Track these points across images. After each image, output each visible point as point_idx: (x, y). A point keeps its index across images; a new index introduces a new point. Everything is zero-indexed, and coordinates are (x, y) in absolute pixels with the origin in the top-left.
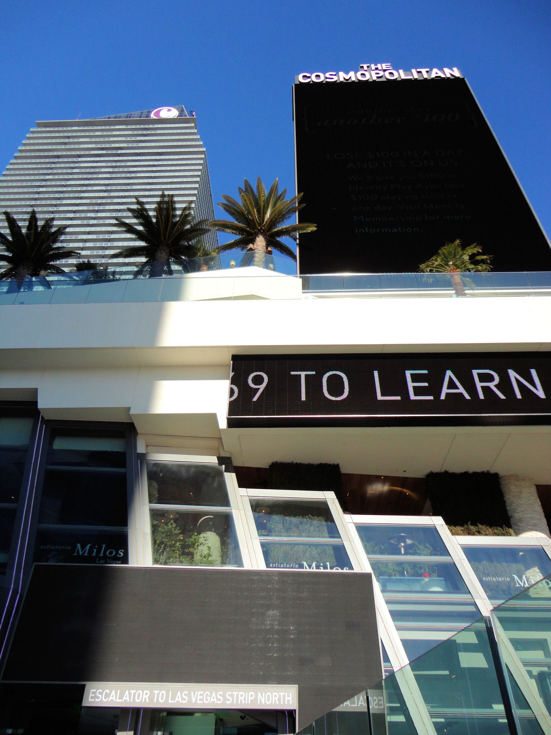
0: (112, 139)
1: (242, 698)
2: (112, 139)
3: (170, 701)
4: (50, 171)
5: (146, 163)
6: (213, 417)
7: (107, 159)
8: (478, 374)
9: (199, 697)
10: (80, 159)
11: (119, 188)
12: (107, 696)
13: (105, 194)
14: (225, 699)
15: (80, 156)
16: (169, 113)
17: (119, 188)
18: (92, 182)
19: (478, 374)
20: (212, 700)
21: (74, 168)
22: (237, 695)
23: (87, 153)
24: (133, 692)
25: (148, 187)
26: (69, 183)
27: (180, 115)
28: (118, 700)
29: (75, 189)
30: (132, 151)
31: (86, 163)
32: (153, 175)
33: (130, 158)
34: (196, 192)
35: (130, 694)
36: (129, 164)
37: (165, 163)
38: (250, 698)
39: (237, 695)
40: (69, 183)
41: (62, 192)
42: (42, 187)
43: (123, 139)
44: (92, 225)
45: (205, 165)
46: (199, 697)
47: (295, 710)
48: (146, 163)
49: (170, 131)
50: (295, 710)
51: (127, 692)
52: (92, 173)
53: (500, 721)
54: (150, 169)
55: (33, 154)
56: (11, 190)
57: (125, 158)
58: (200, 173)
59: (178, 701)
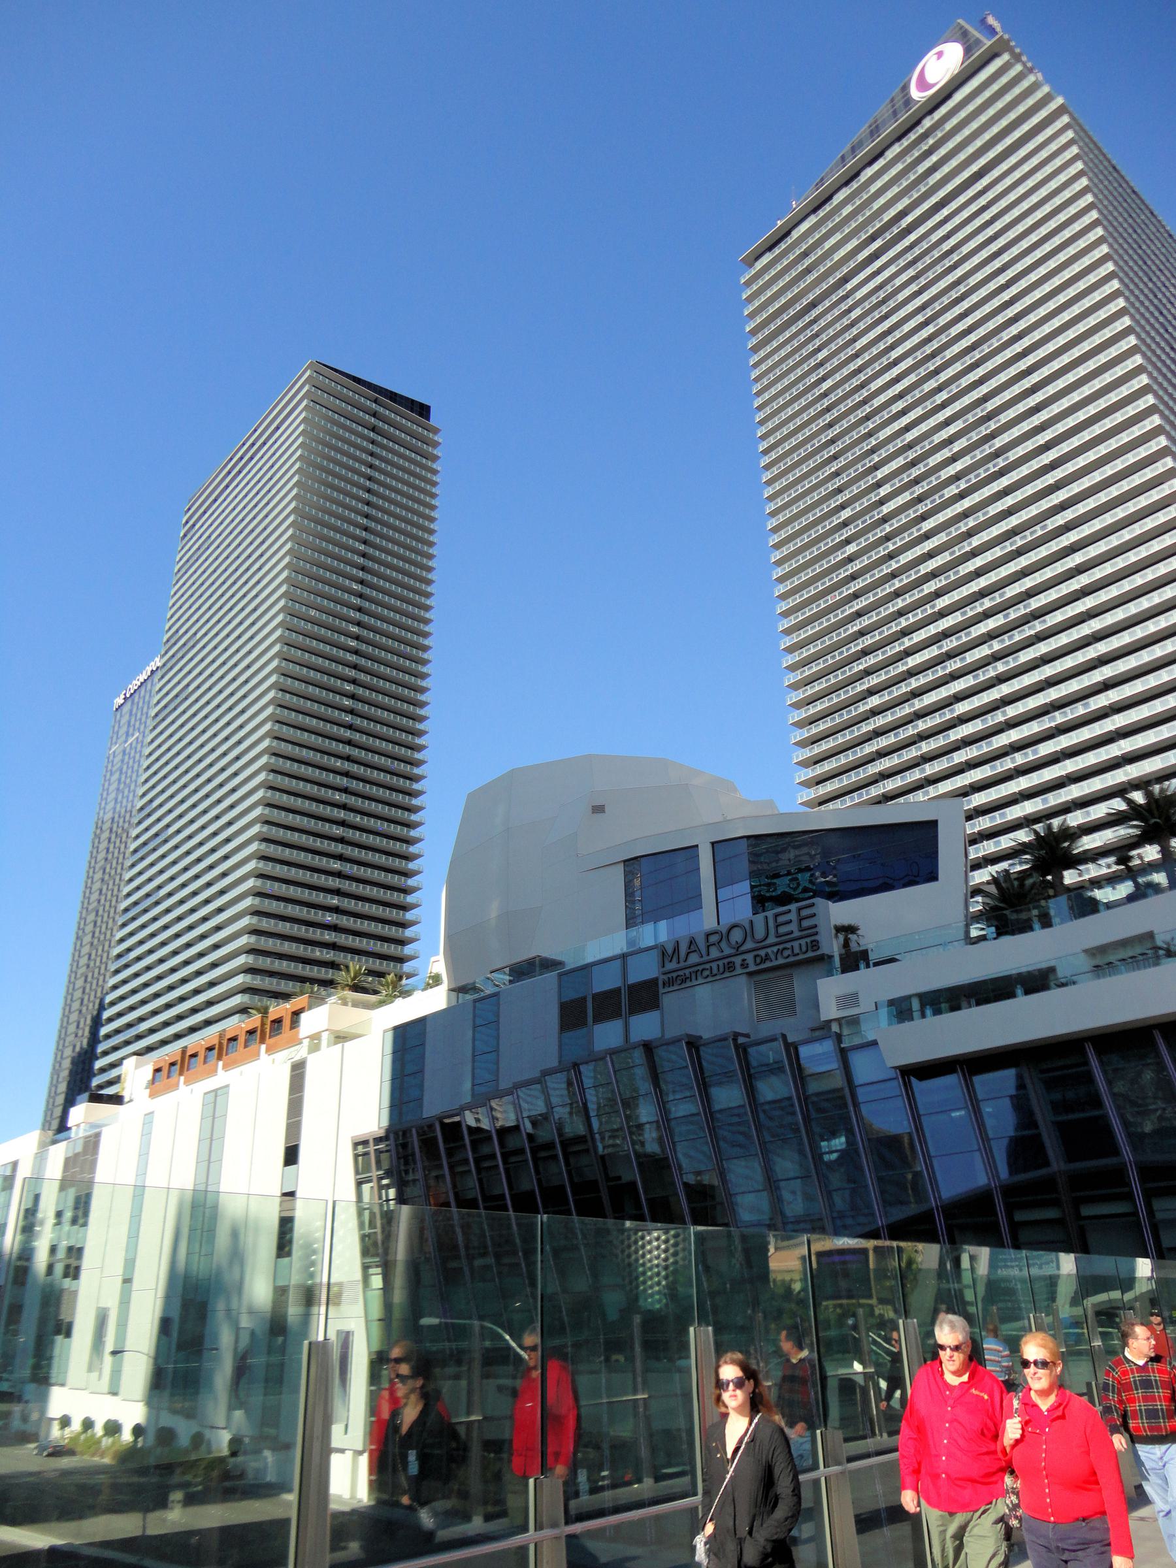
10: (849, 286)
13: (930, 329)
15: (845, 280)
16: (942, 63)
18: (894, 319)
21: (854, 340)
26: (858, 345)
27: (968, 51)
29: (875, 351)
31: (862, 287)
36: (934, 238)
40: (858, 345)
42: (823, 379)
43: (895, 190)
52: (883, 299)
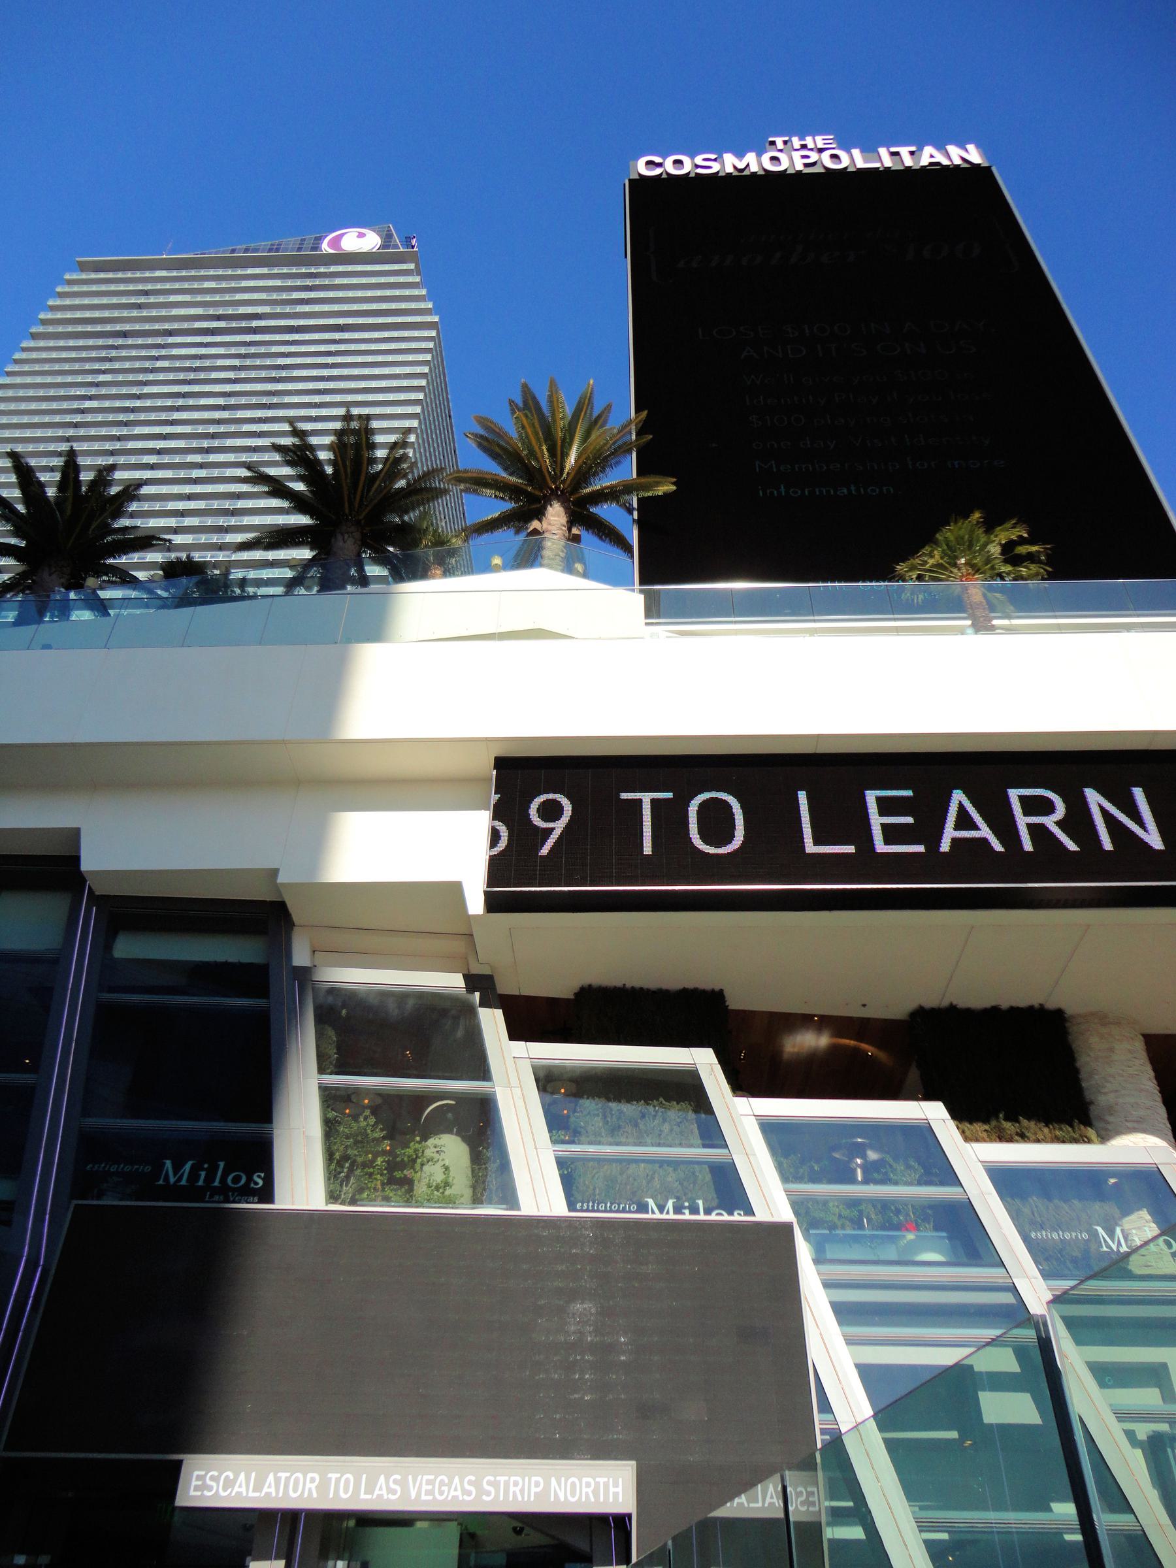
0: (238, 297)
1: (517, 1489)
2: (238, 297)
3: (363, 1496)
4: (107, 365)
5: (313, 348)
6: (454, 890)
7: (228, 338)
8: (1021, 798)
9: (425, 1487)
10: (171, 340)
11: (254, 400)
12: (229, 1484)
13: (225, 415)
14: (481, 1491)
15: (170, 333)
16: (360, 240)
17: (254, 400)
18: (196, 388)
19: (1021, 798)
20: (452, 1493)
21: (157, 358)
22: (507, 1484)
23: (186, 326)
24: (283, 1475)
25: (317, 399)
26: (147, 390)
28: (251, 1494)
29: (159, 403)
30: (282, 323)
31: (183, 348)
32: (326, 372)
33: (277, 337)
34: (418, 410)
35: (277, 1480)
36: (274, 349)
37: (353, 347)
38: (534, 1490)
39: (507, 1484)
40: (147, 390)
41: (133, 410)
42: (90, 398)
43: (263, 296)
44: (197, 481)
45: (437, 352)
46: (425, 1487)
47: (629, 1516)
48: (313, 348)
49: (364, 280)
50: (629, 1516)
51: (271, 1477)
52: (197, 369)
53: (1068, 1537)
54: (319, 360)
55: (70, 329)
56: (23, 406)
57: (267, 338)
58: (426, 370)
59: (380, 1496)
